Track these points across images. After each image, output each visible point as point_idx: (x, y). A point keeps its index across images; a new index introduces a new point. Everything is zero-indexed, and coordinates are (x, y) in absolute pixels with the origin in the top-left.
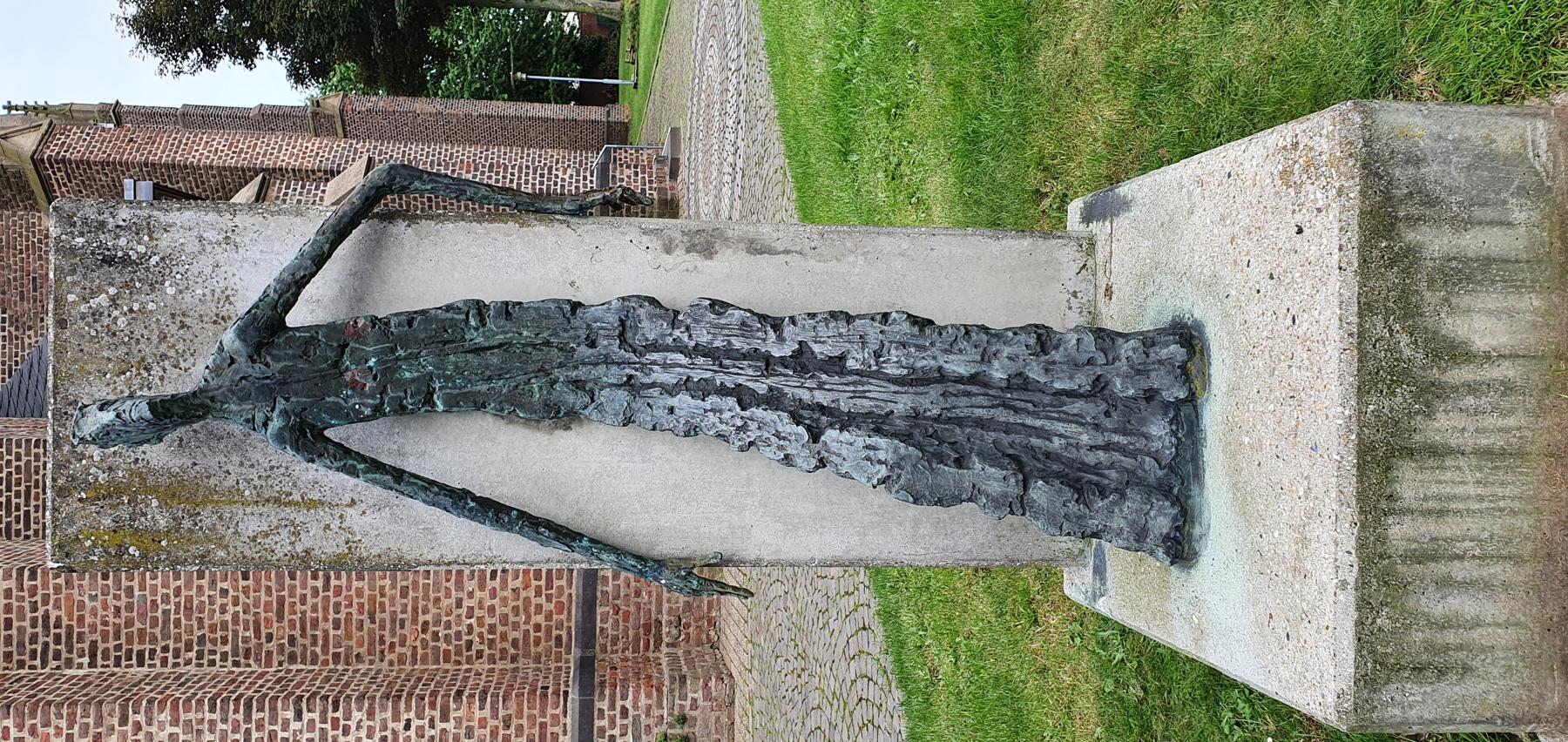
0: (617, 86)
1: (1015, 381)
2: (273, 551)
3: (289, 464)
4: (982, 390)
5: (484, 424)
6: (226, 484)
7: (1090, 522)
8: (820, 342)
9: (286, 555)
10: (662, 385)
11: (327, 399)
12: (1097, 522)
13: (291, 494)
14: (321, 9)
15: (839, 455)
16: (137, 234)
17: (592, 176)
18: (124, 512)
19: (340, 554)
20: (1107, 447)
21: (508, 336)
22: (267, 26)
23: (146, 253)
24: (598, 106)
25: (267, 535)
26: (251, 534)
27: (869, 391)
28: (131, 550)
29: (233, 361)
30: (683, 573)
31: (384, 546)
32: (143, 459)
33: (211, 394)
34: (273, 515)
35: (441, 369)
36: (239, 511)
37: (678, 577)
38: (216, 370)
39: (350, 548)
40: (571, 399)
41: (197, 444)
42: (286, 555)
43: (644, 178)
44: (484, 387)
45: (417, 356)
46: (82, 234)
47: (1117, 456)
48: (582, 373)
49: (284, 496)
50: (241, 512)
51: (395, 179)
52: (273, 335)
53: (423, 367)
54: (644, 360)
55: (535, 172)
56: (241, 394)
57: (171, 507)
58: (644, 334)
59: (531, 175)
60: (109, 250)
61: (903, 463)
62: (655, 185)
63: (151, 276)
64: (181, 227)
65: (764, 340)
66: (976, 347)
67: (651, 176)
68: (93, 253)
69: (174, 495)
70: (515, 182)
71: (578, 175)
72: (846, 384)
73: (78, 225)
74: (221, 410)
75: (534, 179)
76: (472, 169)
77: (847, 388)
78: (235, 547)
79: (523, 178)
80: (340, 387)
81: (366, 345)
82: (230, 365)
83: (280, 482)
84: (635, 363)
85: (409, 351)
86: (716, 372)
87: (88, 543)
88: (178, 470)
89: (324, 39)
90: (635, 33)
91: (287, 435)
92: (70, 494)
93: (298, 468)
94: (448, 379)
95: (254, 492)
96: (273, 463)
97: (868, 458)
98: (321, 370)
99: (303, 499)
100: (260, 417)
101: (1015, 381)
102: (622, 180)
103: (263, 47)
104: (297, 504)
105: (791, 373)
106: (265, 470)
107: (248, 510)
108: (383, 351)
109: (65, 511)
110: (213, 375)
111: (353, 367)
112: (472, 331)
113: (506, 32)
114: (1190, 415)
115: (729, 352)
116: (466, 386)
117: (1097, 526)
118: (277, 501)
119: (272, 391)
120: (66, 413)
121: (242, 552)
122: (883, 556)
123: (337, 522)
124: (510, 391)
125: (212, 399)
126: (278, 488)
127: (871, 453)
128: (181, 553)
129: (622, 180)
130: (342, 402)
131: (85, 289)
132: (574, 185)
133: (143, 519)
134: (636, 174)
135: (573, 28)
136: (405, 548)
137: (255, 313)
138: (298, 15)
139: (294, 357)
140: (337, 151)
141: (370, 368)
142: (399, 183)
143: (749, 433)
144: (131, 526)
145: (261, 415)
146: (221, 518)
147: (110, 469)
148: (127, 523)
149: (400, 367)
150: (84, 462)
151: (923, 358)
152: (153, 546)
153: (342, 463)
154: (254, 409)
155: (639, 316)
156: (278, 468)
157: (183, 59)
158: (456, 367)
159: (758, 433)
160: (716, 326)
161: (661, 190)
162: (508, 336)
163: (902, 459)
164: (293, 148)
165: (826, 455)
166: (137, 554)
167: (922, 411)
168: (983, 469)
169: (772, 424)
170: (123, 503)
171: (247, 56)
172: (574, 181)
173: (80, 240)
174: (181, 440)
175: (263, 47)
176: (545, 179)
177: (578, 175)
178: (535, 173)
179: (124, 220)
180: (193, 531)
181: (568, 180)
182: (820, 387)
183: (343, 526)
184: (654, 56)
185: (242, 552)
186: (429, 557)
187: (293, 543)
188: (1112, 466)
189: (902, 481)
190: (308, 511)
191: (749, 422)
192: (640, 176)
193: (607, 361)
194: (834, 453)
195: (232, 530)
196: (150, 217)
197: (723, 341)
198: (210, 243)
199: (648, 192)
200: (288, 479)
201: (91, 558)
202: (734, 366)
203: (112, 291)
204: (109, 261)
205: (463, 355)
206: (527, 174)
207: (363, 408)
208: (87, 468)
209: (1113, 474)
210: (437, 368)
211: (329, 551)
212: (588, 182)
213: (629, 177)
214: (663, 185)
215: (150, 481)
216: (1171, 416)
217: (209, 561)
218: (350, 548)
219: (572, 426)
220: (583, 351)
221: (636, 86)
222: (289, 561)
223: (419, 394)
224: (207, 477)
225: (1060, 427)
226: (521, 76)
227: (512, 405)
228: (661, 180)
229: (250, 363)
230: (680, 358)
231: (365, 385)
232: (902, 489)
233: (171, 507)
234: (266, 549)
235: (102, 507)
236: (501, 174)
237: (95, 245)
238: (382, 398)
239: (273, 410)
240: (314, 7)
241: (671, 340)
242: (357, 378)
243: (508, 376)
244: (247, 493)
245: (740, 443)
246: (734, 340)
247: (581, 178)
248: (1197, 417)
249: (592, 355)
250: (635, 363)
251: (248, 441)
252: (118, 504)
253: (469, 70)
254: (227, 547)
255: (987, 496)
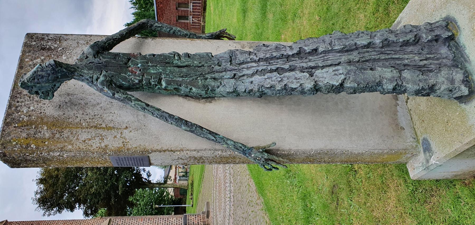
0: (185, 207)
1: (385, 42)
2: (92, 146)
3: (102, 114)
4: (373, 50)
5: (179, 101)
6: (76, 121)
7: (430, 81)
8: (307, 46)
9: (97, 147)
10: (247, 75)
11: (122, 74)
12: (433, 81)
13: (102, 125)
14: (96, 191)
15: (323, 77)
16: (55, 41)
17: (181, 219)
18: (32, 132)
19: (120, 147)
20: (426, 59)
21: (189, 63)
22: (79, 197)
23: (57, 47)
24: (180, 214)
25: (90, 140)
26: (83, 139)
27: (329, 58)
28: (32, 146)
29: (87, 57)
30: (261, 150)
31: (138, 144)
32: (44, 112)
33: (77, 66)
34: (93, 132)
35: (165, 71)
36: (79, 131)
37: (259, 152)
38: (81, 60)
39: (124, 145)
40: (213, 84)
41: (66, 107)
42: (97, 147)
43: (198, 219)
44: (181, 79)
45: (156, 66)
46: (35, 41)
47: (431, 61)
48: (216, 75)
49: (99, 125)
50: (80, 132)
51: (149, 22)
52: (103, 50)
53: (158, 70)
54: (240, 68)
55: (163, 220)
56: (89, 68)
57: (52, 130)
58: (239, 59)
59: (162, 221)
60: (44, 46)
61: (350, 73)
62: (202, 221)
63: (58, 53)
64: (71, 39)
65: (285, 51)
66: (367, 35)
67: (200, 218)
68: (38, 47)
69: (54, 125)
70: (157, 223)
71: (177, 219)
72: (320, 58)
73: (34, 39)
74: (80, 71)
75: (163, 222)
76: (143, 220)
77: (320, 59)
78: (76, 145)
79: (159, 222)
80: (127, 71)
81: (137, 60)
82: (86, 58)
83: (98, 120)
84: (237, 69)
85: (153, 64)
86: (268, 65)
87: (14, 143)
88: (57, 116)
89: (96, 200)
90: (192, 189)
91: (105, 83)
92: (11, 125)
93: (105, 115)
94: (167, 75)
95: (87, 124)
96: (95, 114)
97: (336, 74)
98: (120, 64)
99: (106, 126)
100: (95, 77)
101: (385, 42)
102: (191, 220)
103: (77, 206)
104: (104, 128)
105: (297, 59)
106: (92, 116)
107: (83, 130)
108: (143, 62)
109: (7, 131)
110: (79, 61)
111: (132, 66)
112: (176, 61)
113: (152, 198)
114: (454, 44)
115: (272, 58)
116: (173, 78)
117: (433, 82)
118: (96, 127)
119: (101, 68)
120: (16, 97)
121: (79, 146)
122: (341, 148)
123: (120, 135)
124: (190, 81)
125: (78, 67)
126: (96, 123)
127: (336, 72)
128: (53, 147)
129: (191, 220)
130: (127, 76)
131: (33, 57)
132: (176, 222)
133: (39, 134)
134: (196, 218)
135: (172, 196)
136: (147, 144)
137: (97, 43)
138: (89, 193)
139: (110, 58)
140: (99, 223)
141: (139, 67)
142: (150, 23)
143: (284, 82)
144: (34, 136)
145: (96, 76)
146: (72, 133)
147: (30, 116)
148: (32, 135)
149: (150, 68)
150: (19, 113)
151: (348, 41)
152: (41, 144)
153: (126, 96)
154: (93, 73)
155: (236, 54)
156: (97, 115)
157: (52, 210)
158: (170, 71)
159: (288, 80)
160: (266, 51)
161: (204, 222)
162: (189, 63)
163: (349, 71)
164: (85, 223)
165: (317, 79)
166: (34, 147)
167: (352, 60)
168: (382, 70)
169: (293, 76)
170: (32, 128)
171: (72, 209)
172: (176, 221)
173: (34, 43)
174: (60, 106)
175: (77, 206)
176: (166, 222)
177: (177, 219)
178: (163, 220)
179: (51, 38)
180: (59, 138)
181: (174, 221)
182: (310, 61)
183: (122, 136)
184: (199, 191)
185: (79, 146)
186: (157, 148)
187: (101, 143)
188: (431, 64)
189: (351, 79)
190: (108, 131)
191: (284, 78)
192: (197, 218)
193: (225, 70)
194: (321, 77)
195: (76, 138)
196: (61, 37)
197: (269, 55)
198: (81, 44)
199: (200, 223)
200: (101, 119)
201: (14, 149)
202: (275, 62)
203: (42, 58)
204: (43, 49)
205: (173, 67)
206: (160, 221)
207: (135, 80)
208: (20, 115)
209: (432, 66)
210: (163, 71)
211: (115, 146)
212: (180, 221)
213: (193, 219)
214: (204, 220)
215: (45, 120)
216: (447, 45)
217: (65, 150)
218: (124, 145)
219: (212, 102)
220: (217, 68)
221: (192, 206)
222: (98, 150)
223: (156, 78)
224: (68, 119)
225: (406, 56)
226: (157, 206)
227: (191, 86)
228: (204, 218)
229: (94, 58)
230: (254, 64)
231: (136, 72)
232: (352, 82)
233: (52, 130)
234: (89, 145)
235: (23, 130)
236: (152, 221)
237: (39, 44)
238: (142, 78)
239: (100, 75)
240: (95, 190)
241: (249, 59)
242: (134, 70)
243: (189, 76)
244: (84, 124)
245: (281, 86)
246: (273, 53)
247: (178, 220)
248: (457, 44)
249: (220, 69)
250: (237, 69)
251: (87, 106)
252: (30, 129)
253: (140, 210)
254: (73, 144)
255: (386, 79)
